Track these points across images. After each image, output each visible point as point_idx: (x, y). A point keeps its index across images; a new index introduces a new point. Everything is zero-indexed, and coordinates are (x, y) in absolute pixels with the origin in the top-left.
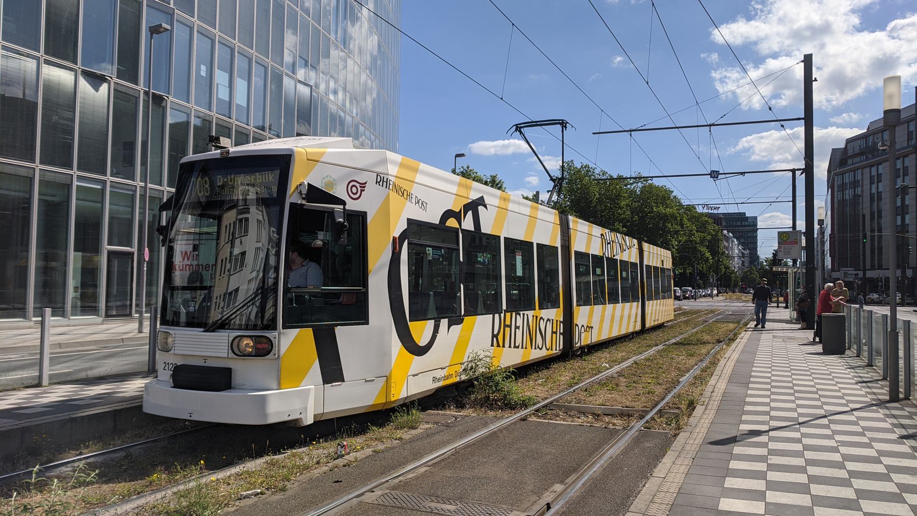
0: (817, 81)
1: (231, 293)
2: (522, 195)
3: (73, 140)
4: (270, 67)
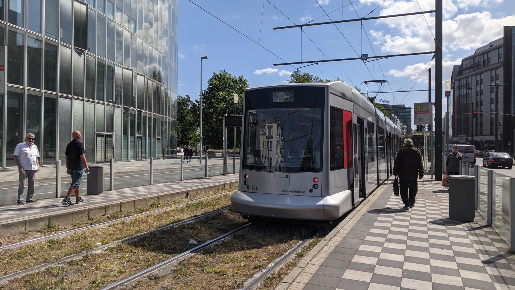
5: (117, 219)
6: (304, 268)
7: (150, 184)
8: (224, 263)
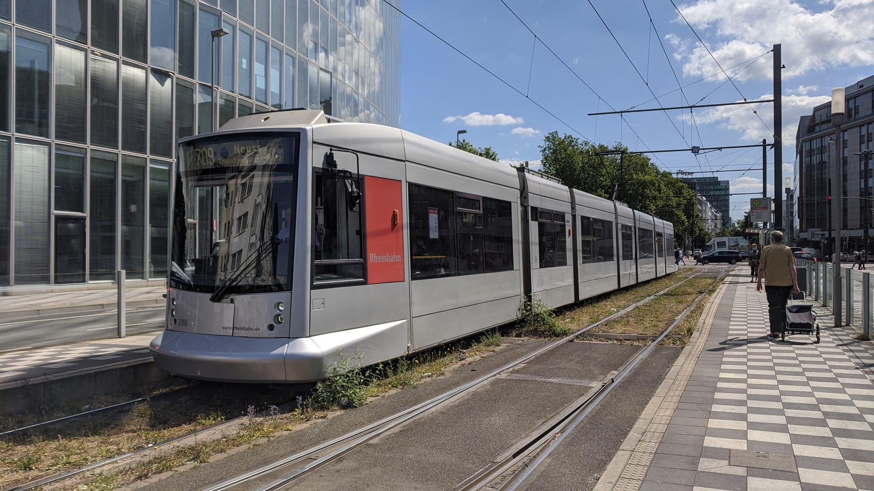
0: (785, 67)
1: (234, 255)
2: (510, 165)
3: (146, 129)
4: (284, 51)
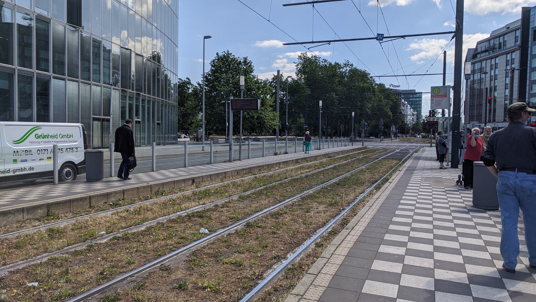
2: (273, 75)
5: (121, 206)
6: (329, 258)
7: (153, 171)
8: (240, 253)
